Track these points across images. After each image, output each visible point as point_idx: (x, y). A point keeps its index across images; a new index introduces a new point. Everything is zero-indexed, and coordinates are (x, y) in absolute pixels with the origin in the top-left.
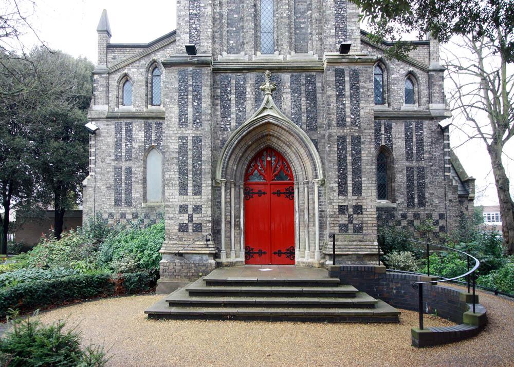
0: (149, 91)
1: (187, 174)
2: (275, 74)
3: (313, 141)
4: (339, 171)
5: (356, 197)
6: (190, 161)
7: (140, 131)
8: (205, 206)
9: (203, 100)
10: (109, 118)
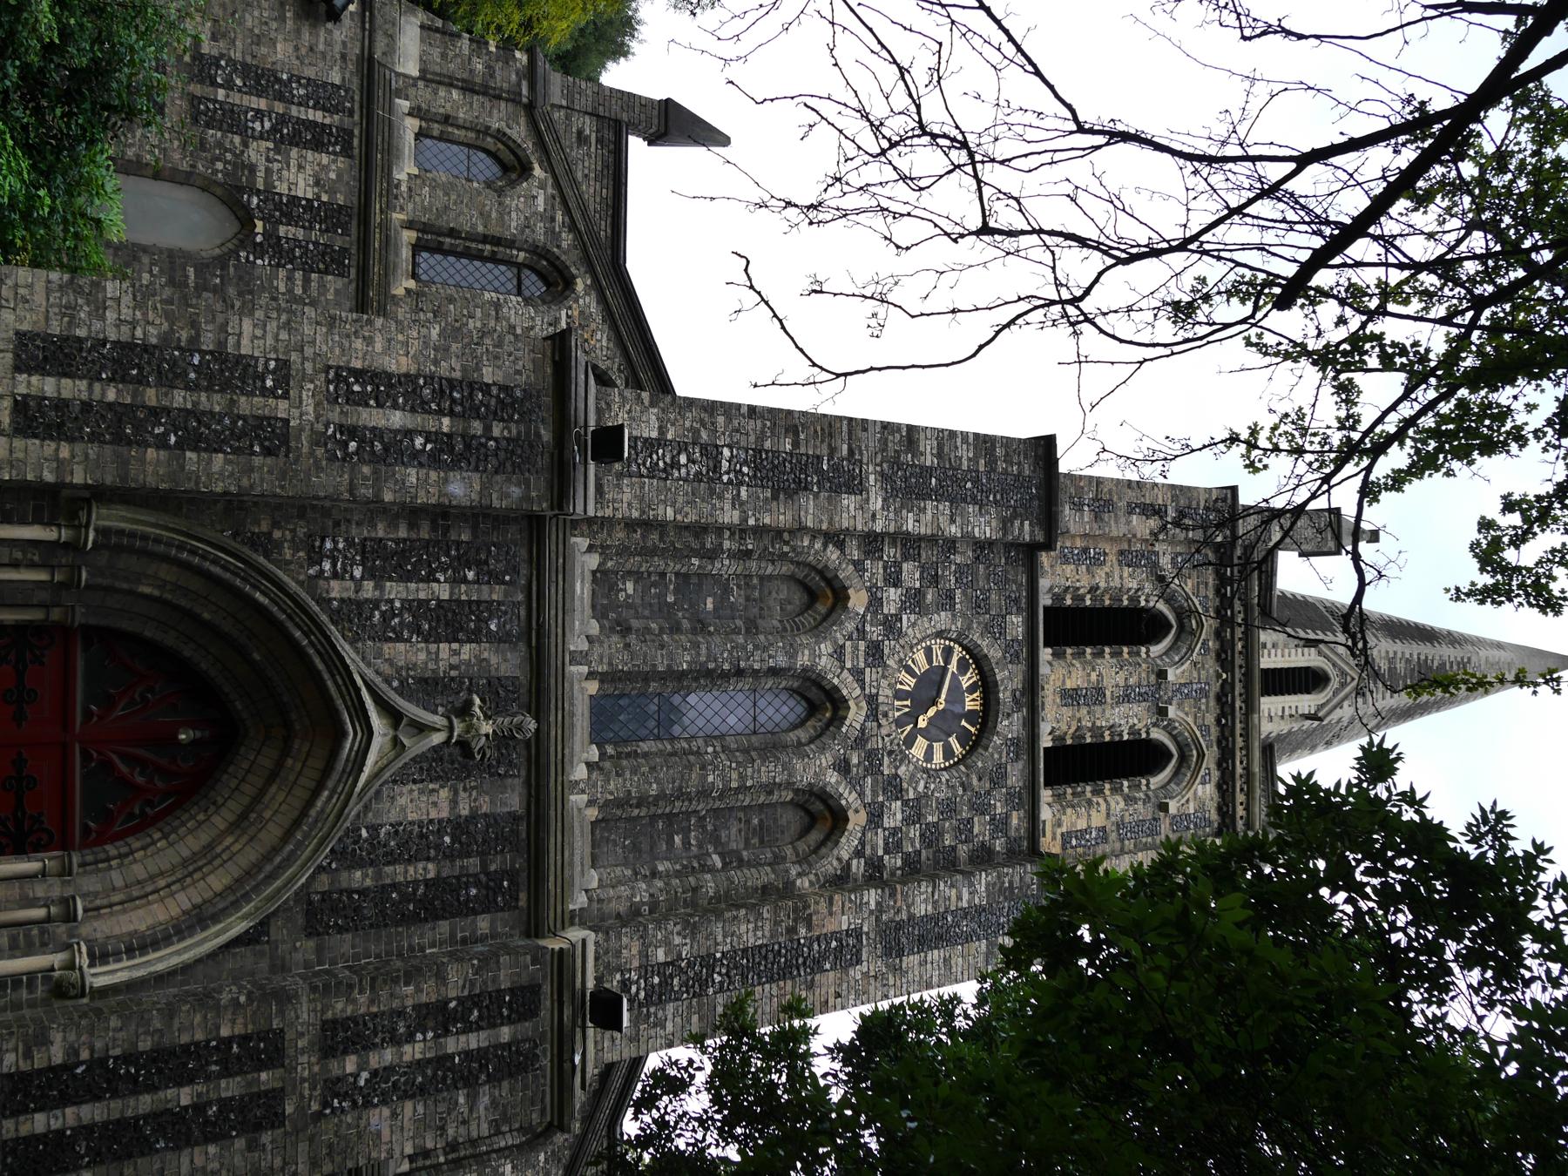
1: (119, 377)
2: (524, 753)
3: (261, 923)
4: (128, 1058)
6: (179, 399)
7: (317, 183)
9: (433, 475)
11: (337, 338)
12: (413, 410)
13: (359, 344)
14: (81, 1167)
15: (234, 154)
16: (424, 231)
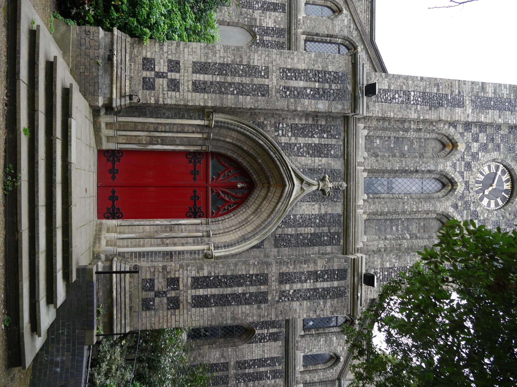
3: (261, 242)
4: (224, 277)
6: (237, 80)
9: (313, 102)
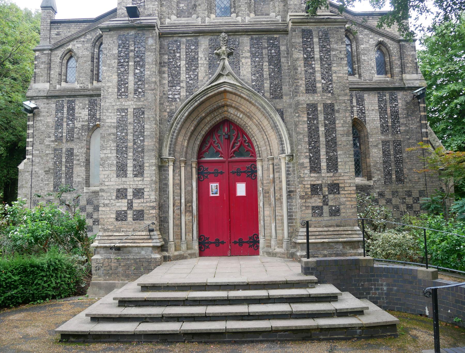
0: (95, 66)
2: (232, 36)
3: (277, 111)
4: (310, 144)
5: (332, 174)
6: (130, 137)
7: (84, 109)
8: (148, 190)
9: (147, 66)
10: (47, 97)
11: (109, 96)
12: (128, 73)
13: (110, 90)
14: (337, 154)
15: (80, 130)
16: (93, 79)
